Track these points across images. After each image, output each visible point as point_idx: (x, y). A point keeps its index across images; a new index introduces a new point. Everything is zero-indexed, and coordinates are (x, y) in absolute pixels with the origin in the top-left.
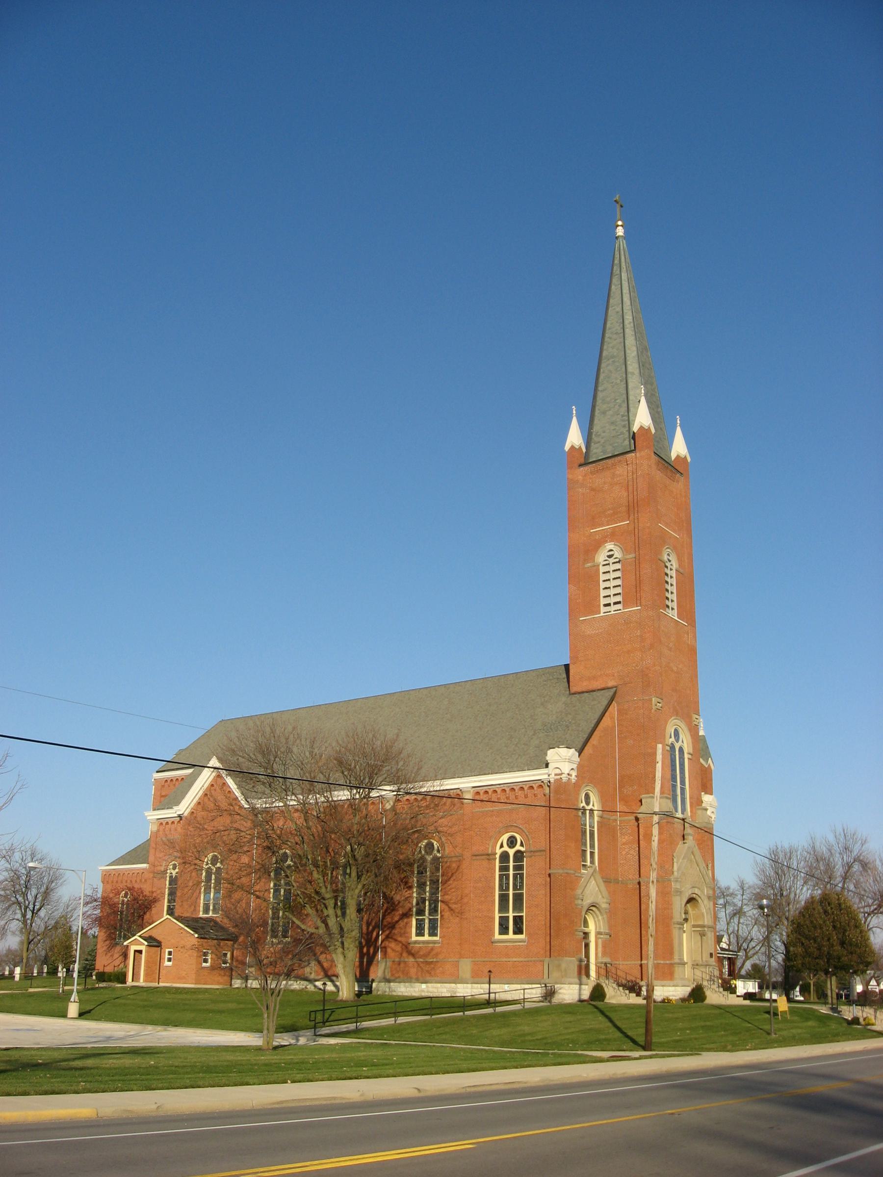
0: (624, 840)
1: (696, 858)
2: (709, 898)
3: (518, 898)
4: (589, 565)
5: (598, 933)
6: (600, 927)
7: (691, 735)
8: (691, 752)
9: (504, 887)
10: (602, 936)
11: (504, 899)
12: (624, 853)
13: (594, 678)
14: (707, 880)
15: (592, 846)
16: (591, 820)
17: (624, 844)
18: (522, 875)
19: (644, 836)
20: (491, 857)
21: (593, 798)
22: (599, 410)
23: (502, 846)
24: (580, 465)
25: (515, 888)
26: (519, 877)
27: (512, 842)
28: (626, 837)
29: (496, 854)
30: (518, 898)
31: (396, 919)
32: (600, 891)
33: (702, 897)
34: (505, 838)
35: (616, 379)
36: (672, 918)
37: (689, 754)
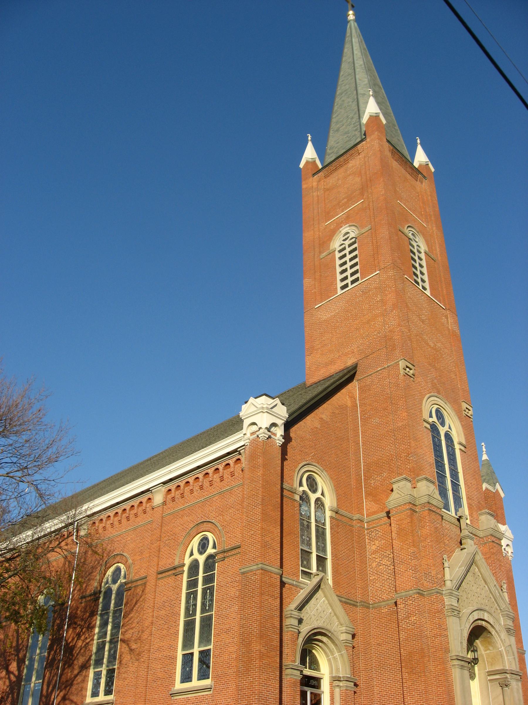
0: (374, 548)
1: (482, 570)
2: (508, 630)
3: (206, 623)
4: (324, 254)
5: (335, 679)
6: (337, 670)
7: (462, 426)
8: (464, 442)
9: (190, 611)
10: (341, 684)
11: (189, 626)
12: (374, 564)
13: (332, 362)
14: (503, 606)
15: (321, 548)
16: (318, 514)
17: (375, 552)
18: (211, 589)
19: (398, 534)
20: (178, 570)
21: (321, 483)
22: (333, 131)
23: (192, 554)
24: (314, 175)
25: (203, 610)
26: (208, 592)
27: (203, 546)
28: (377, 542)
29: (184, 565)
30: (206, 623)
31: (76, 672)
32: (335, 614)
33: (497, 627)
34: (195, 542)
35: (349, 102)
36: (447, 650)
37: (460, 444)
